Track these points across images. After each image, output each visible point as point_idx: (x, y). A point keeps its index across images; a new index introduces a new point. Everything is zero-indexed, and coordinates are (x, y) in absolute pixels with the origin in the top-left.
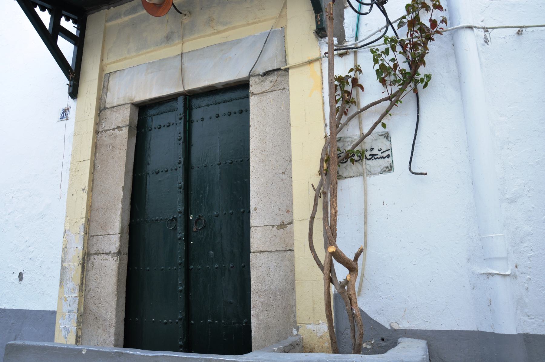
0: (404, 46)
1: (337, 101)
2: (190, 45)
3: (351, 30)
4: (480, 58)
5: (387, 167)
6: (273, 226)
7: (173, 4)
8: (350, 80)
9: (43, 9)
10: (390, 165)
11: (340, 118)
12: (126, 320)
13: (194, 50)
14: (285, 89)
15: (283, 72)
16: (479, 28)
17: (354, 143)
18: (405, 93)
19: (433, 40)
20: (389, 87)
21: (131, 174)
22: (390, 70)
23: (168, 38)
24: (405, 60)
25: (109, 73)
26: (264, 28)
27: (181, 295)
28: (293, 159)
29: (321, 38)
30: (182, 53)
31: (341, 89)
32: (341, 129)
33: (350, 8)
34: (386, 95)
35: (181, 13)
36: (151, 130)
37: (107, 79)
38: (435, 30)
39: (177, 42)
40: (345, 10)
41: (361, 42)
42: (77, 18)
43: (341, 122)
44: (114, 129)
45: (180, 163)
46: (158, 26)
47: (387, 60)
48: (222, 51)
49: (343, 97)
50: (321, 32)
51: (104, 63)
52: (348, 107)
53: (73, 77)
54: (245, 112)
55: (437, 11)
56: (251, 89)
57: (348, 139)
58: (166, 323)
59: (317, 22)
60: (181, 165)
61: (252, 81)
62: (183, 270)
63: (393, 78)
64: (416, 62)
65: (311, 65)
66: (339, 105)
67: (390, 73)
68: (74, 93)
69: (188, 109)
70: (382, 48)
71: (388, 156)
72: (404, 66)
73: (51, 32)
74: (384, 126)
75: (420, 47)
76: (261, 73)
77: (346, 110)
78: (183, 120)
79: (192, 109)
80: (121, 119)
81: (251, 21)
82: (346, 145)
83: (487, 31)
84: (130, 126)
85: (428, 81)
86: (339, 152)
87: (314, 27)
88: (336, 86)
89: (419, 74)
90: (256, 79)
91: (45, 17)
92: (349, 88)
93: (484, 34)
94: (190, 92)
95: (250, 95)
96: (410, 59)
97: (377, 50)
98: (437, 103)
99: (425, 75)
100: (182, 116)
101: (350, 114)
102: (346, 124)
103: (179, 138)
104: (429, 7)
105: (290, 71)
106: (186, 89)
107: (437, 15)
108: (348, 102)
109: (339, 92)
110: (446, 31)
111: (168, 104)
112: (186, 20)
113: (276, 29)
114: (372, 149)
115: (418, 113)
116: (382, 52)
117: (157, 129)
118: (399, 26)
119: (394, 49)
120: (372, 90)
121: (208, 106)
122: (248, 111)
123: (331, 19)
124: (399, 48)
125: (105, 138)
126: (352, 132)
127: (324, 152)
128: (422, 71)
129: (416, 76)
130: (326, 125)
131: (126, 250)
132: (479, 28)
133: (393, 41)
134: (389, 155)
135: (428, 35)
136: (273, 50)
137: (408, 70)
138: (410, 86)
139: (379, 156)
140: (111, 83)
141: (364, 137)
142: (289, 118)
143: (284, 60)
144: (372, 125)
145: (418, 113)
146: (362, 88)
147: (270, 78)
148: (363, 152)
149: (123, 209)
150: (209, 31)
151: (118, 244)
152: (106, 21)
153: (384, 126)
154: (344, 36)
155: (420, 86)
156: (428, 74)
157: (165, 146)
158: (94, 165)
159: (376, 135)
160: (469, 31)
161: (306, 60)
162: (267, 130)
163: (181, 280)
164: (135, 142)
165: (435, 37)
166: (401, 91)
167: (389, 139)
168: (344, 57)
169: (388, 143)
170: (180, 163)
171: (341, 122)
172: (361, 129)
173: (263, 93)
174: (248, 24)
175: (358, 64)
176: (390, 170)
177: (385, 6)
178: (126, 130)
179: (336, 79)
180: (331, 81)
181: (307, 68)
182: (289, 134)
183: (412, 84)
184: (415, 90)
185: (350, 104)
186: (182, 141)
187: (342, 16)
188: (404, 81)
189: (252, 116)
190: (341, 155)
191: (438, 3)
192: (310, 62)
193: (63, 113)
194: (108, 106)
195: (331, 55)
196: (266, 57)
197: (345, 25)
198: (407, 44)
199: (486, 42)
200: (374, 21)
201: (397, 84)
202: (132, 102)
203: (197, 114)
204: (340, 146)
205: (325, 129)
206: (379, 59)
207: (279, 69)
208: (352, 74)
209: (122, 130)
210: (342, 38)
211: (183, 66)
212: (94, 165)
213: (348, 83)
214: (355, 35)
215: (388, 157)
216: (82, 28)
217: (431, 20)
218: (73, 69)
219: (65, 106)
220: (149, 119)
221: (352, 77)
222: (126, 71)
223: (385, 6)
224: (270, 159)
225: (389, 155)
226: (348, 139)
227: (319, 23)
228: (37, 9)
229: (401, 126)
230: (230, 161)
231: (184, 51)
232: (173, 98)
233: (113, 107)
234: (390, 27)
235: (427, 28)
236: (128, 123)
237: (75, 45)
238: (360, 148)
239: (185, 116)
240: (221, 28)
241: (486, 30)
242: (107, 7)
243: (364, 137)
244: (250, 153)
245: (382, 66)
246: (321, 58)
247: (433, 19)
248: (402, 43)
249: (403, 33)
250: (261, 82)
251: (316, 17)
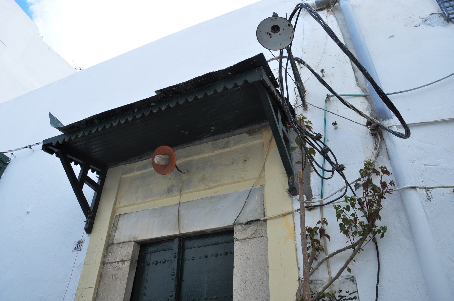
0: (361, 204)
1: (308, 248)
2: (186, 197)
3: (317, 189)
4: (425, 212)
7: (176, 166)
8: (318, 231)
9: (76, 164)
11: (311, 263)
13: (190, 201)
14: (264, 237)
15: (262, 222)
16: (421, 188)
17: (324, 286)
18: (365, 242)
19: (385, 198)
20: (351, 238)
22: (351, 222)
23: (170, 190)
24: (363, 214)
25: (119, 215)
26: (247, 186)
28: (271, 298)
29: (293, 195)
30: (180, 203)
31: (311, 239)
32: (313, 273)
33: (315, 172)
34: (349, 244)
35: (181, 172)
36: (149, 265)
37: (117, 219)
38: (385, 190)
39: (176, 194)
40: (311, 173)
41: (325, 199)
42: (100, 170)
43: (312, 266)
44: (118, 262)
45: (171, 296)
46: (162, 182)
47: (348, 215)
48: (212, 203)
49: (313, 245)
50: (292, 191)
51: (116, 206)
52: (317, 253)
53: (91, 216)
54: (230, 254)
55: (385, 176)
56: (236, 235)
57: (319, 282)
59: (289, 183)
60: (173, 298)
61: (236, 229)
63: (354, 229)
64: (373, 216)
65: (285, 217)
66: (310, 251)
67: (351, 225)
68: (89, 229)
69: (182, 249)
70: (344, 205)
72: (362, 218)
73: (79, 181)
74: (349, 270)
75: (374, 204)
76: (244, 223)
77: (315, 256)
78: (176, 259)
79: (185, 250)
80: (125, 253)
81: (236, 180)
82: (317, 287)
83: (428, 190)
84: (132, 261)
85: (384, 232)
86: (311, 293)
87: (287, 187)
88: (307, 235)
89: (376, 227)
90: (240, 227)
91: (77, 169)
92: (317, 237)
93: (425, 192)
94: (184, 235)
95: (234, 240)
96: (368, 214)
97: (340, 206)
98: (393, 250)
99: (381, 227)
100: (176, 255)
101: (320, 259)
102: (317, 269)
103: (172, 274)
104: (379, 172)
105: (268, 222)
106: (181, 233)
107: (386, 179)
108: (317, 249)
109: (309, 241)
110: (395, 190)
111: (165, 244)
112: (184, 177)
113: (257, 187)
114: (340, 291)
115: (378, 259)
116: (344, 208)
117: (154, 264)
118: (357, 186)
119: (353, 206)
120: (337, 241)
121: (199, 247)
122: (232, 253)
123: (302, 183)
124: (357, 206)
125: (110, 269)
126: (322, 276)
127: (299, 294)
128: (378, 223)
129: (373, 228)
130: (299, 269)
132: (421, 188)
133: (352, 200)
134: (356, 297)
135: (380, 193)
136: (253, 204)
137: (366, 223)
138: (370, 236)
139: (347, 298)
140: (120, 223)
141: (332, 281)
142: (267, 261)
143: (263, 212)
144: (339, 270)
145: (378, 259)
146: (328, 237)
148: (333, 295)
150: (203, 187)
152: (122, 174)
153: (349, 270)
154: (311, 194)
155: (378, 236)
156: (383, 226)
157: (160, 275)
158: (97, 292)
159: (343, 278)
160: (413, 191)
161: (281, 213)
162: (248, 271)
165: (386, 195)
166: (362, 240)
167: (355, 282)
168: (312, 211)
169: (354, 286)
170: (171, 296)
171: (312, 266)
172: (329, 273)
173: (245, 239)
174: (234, 183)
175: (324, 217)
177: (343, 171)
178: (128, 264)
179: (307, 230)
180: (303, 233)
181: (282, 220)
182: (268, 276)
183: (370, 234)
184: (374, 240)
185: (319, 251)
186: (175, 277)
187: (309, 178)
188: (364, 232)
189: (235, 259)
190: (313, 296)
191: (385, 169)
192: (284, 215)
193: (77, 245)
194: (115, 242)
195: (302, 212)
197: (312, 185)
198: (364, 201)
199: (429, 199)
200: (335, 183)
201: (358, 235)
202: (136, 240)
203: (189, 254)
204: (312, 288)
205: (298, 273)
206: (342, 215)
207: (259, 220)
208: (320, 226)
209: (124, 264)
210: (310, 196)
211: (180, 213)
212: (97, 292)
213: (316, 233)
214: (320, 193)
215: (355, 299)
216: (102, 178)
217: (381, 183)
218: (92, 209)
219: (79, 239)
220: (148, 256)
221: (320, 228)
222: (133, 214)
223: (343, 171)
224: (251, 297)
225: (356, 297)
226: (319, 282)
227: (291, 184)
228: (72, 164)
229: (364, 268)
230: (215, 297)
231: (181, 202)
233: (120, 243)
234: (348, 187)
235: (379, 188)
236: (130, 258)
237: (95, 191)
238: (330, 290)
239: (179, 255)
240: (212, 185)
241: (427, 189)
242: (124, 163)
243: (332, 281)
244: (234, 291)
245: (345, 220)
246: (293, 212)
247: (383, 181)
248: (359, 200)
249: (360, 193)
250: (244, 230)
251: (289, 179)
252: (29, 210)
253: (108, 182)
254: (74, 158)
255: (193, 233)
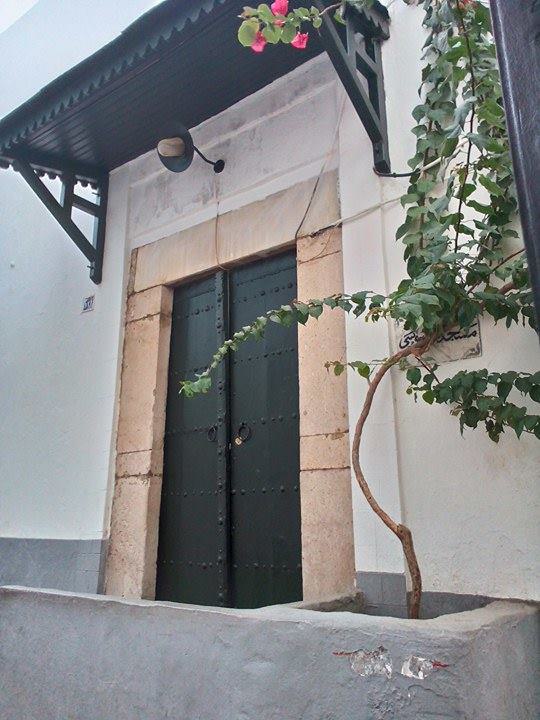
5: (474, 350)
6: (327, 435)
10: (478, 346)
12: (160, 563)
21: (165, 374)
27: (222, 529)
44: (144, 318)
58: (205, 568)
61: (299, 244)
62: (224, 494)
68: (97, 278)
71: (474, 334)
78: (221, 304)
105: (344, 228)
131: (160, 471)
147: (321, 239)
149: (155, 419)
151: (149, 463)
163: (221, 508)
164: (169, 332)
176: (477, 353)
196: (315, 212)
203: (241, 291)
216: (104, 195)
228: (45, 179)
232: (209, 275)
233: (143, 291)
236: (159, 310)
239: (225, 297)
251: (374, 147)
252: (13, 263)
253: (116, 199)
254: (47, 169)
255: (241, 260)
